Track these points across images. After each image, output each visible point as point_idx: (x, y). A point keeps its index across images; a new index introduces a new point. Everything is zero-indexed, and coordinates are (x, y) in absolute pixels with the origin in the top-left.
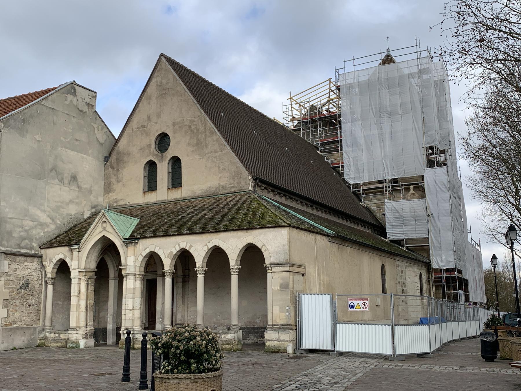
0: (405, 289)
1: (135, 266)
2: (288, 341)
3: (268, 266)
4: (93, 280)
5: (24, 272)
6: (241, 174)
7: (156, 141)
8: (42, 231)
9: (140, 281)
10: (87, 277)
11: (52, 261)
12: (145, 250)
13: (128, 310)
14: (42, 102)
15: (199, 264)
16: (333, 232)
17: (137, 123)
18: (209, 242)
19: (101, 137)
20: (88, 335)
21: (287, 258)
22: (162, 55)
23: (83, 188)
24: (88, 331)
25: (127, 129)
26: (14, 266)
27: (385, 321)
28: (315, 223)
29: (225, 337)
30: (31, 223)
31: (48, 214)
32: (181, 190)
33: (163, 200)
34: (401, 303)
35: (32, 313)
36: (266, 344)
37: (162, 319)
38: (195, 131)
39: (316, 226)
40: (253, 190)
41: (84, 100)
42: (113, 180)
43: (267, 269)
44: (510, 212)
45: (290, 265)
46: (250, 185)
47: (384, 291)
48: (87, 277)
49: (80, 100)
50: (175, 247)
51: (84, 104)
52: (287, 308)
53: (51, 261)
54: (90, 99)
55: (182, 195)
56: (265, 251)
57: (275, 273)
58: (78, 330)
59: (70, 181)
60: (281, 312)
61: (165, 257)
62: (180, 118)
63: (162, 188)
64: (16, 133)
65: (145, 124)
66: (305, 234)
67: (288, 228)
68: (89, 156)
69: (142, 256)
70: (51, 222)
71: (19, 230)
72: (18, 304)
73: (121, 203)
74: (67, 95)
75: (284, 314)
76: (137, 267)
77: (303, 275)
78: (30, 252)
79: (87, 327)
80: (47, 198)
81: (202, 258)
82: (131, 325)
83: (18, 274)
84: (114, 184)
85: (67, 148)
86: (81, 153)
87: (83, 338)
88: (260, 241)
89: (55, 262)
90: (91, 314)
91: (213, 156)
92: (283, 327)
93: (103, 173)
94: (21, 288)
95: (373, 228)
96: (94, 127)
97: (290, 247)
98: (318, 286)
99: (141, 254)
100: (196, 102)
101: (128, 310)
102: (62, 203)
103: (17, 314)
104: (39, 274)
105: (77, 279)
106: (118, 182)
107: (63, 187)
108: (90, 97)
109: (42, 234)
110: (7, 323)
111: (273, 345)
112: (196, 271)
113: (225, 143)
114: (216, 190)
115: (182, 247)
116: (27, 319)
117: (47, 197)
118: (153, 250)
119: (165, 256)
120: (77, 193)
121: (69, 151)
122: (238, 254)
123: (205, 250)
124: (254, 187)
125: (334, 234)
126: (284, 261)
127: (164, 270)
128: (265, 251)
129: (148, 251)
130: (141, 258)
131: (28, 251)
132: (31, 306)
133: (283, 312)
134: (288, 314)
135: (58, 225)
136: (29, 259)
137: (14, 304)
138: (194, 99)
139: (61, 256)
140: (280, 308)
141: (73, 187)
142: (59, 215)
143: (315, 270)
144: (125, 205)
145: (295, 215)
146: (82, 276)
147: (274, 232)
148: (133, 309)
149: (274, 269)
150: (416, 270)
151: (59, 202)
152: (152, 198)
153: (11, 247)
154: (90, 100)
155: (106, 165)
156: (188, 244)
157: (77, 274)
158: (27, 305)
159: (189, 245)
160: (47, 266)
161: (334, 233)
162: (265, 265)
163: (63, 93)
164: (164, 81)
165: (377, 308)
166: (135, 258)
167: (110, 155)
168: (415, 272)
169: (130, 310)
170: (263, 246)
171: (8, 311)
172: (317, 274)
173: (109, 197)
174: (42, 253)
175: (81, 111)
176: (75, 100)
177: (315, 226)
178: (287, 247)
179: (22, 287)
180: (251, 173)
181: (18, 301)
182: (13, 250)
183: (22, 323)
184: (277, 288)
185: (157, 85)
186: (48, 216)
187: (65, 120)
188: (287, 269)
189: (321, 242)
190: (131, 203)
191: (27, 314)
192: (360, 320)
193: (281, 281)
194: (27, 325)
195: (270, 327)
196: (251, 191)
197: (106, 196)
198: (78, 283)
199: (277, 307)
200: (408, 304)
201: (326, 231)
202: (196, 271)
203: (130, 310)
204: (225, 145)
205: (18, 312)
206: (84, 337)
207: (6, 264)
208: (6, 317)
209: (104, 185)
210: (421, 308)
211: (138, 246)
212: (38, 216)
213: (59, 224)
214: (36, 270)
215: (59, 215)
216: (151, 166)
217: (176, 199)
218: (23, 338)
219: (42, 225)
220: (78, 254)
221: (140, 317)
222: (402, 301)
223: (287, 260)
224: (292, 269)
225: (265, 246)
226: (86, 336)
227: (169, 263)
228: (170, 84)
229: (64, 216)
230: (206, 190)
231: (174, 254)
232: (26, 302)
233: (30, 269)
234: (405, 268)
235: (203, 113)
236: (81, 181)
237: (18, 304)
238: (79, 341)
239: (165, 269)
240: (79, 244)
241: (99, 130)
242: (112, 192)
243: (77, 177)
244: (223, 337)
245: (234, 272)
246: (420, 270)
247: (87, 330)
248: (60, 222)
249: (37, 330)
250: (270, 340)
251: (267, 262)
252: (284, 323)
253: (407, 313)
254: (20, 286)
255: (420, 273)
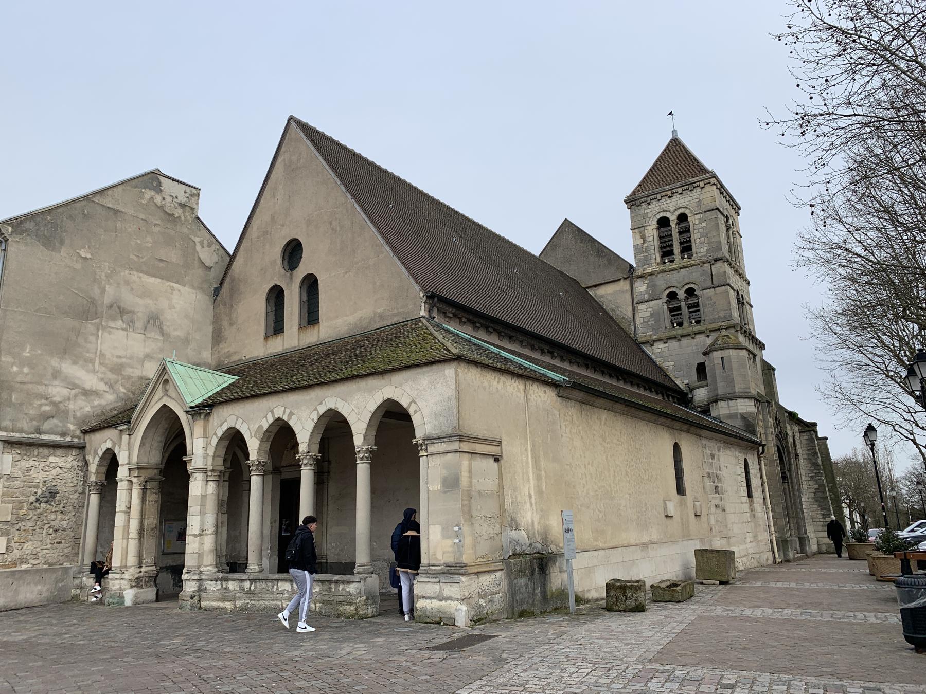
0: (720, 485)
1: (206, 456)
2: (457, 600)
3: (420, 442)
4: (155, 484)
5: (48, 473)
6: (408, 290)
7: (284, 255)
8: (89, 405)
9: (215, 482)
10: (142, 478)
11: (97, 454)
12: (221, 425)
13: (192, 535)
14: (94, 197)
15: (358, 440)
16: (565, 378)
17: (258, 229)
18: (321, 403)
19: (208, 256)
20: (142, 581)
21: (454, 425)
22: (291, 118)
23: (171, 336)
24: (141, 574)
25: (244, 241)
26: (25, 464)
27: (685, 542)
28: (531, 364)
29: (344, 589)
30: (65, 392)
31: (100, 375)
32: (319, 328)
33: (292, 348)
34: (713, 509)
35: (60, 543)
36: (417, 605)
37: (270, 549)
38: (338, 229)
39: (533, 368)
40: (427, 316)
41: (175, 200)
42: (225, 323)
43: (419, 448)
44: (884, 363)
45: (462, 438)
46: (423, 308)
47: (681, 490)
48: (142, 478)
49: (169, 199)
50: (266, 417)
51: (177, 205)
52: (456, 529)
53: (96, 453)
54: (188, 197)
55: (319, 337)
56: (415, 412)
57: (434, 457)
58: (124, 573)
59: (147, 324)
60: (445, 537)
61: (251, 437)
62: (316, 211)
63: (291, 327)
64: (38, 243)
65: (268, 229)
66: (499, 379)
67: (455, 364)
68: (184, 286)
69: (217, 437)
70: (105, 388)
71: (39, 403)
72: (31, 528)
73: (235, 358)
74: (143, 190)
75: (449, 542)
76: (209, 458)
77: (497, 460)
78: (62, 439)
79: (140, 567)
80: (101, 351)
81: (309, 434)
82: (196, 564)
83: (33, 476)
84: (225, 329)
85: (142, 272)
86: (169, 280)
87: (132, 587)
88: (405, 394)
89: (100, 453)
90: (151, 543)
91: (365, 266)
92: (449, 568)
93: (210, 314)
94: (37, 500)
95: (666, 393)
96: (194, 241)
97: (459, 399)
98: (532, 482)
99: (215, 434)
100: (339, 182)
101: (192, 535)
102: (131, 358)
103: (28, 547)
104: (79, 475)
105: (126, 482)
106: (231, 324)
107: (132, 334)
108: (187, 195)
109: (88, 409)
110: (7, 563)
111: (428, 608)
112: (299, 460)
113: (382, 241)
114: (370, 323)
115: (277, 416)
116: (52, 555)
117: (99, 349)
118: (233, 425)
119: (251, 434)
120: (160, 345)
121: (145, 276)
122: (367, 422)
123: (313, 420)
124: (429, 311)
125: (567, 382)
126: (450, 431)
127: (249, 460)
128: (415, 412)
129: (225, 427)
130: (215, 441)
131: (58, 438)
132: (60, 531)
133: (449, 537)
134: (458, 541)
135: (122, 395)
136: (59, 452)
137: (22, 528)
138: (336, 178)
139: (109, 445)
140: (443, 529)
141: (153, 334)
142: (122, 379)
143: (526, 450)
144: (240, 360)
145: (498, 353)
146: (135, 477)
147: (430, 374)
148: (200, 535)
149: (431, 449)
150: (737, 454)
151: (124, 357)
152: (278, 345)
153: (21, 431)
154: (186, 200)
155: (216, 301)
156: (287, 410)
157: (127, 473)
158: (51, 530)
159: (288, 411)
160: (91, 462)
161: (567, 379)
162: (414, 441)
163: (136, 187)
164: (294, 158)
165: (669, 521)
166: (207, 441)
167: (221, 284)
168: (736, 457)
169: (195, 536)
170: (411, 403)
171: (9, 541)
172: (532, 458)
173: (220, 349)
174: (86, 441)
175: (169, 215)
176: (158, 199)
177: (531, 369)
178: (454, 402)
179: (41, 499)
180: (423, 289)
181: (30, 524)
182: (26, 436)
183: (39, 562)
184: (436, 486)
185: (285, 165)
186: (102, 380)
187: (139, 229)
188: (455, 446)
189: (539, 396)
190: (247, 357)
191: (49, 546)
192: (634, 544)
193: (445, 472)
194: (51, 565)
195: (425, 570)
196: (424, 317)
197: (215, 349)
198: (128, 489)
199: (436, 526)
200: (728, 510)
201: (553, 377)
202: (299, 460)
203: (195, 536)
204: (382, 245)
205: (30, 543)
206: (134, 584)
207: (6, 461)
208: (4, 552)
209: (213, 332)
210: (750, 516)
211: (211, 419)
212: (79, 378)
213: (123, 392)
214: (72, 470)
215: (122, 379)
216: (276, 296)
217: (311, 343)
218: (39, 587)
219: (87, 393)
220: (129, 439)
221: (214, 548)
222: (716, 506)
223: (455, 427)
224: (465, 446)
225: (415, 403)
226: (138, 582)
227: (257, 447)
228: (302, 161)
229: (133, 380)
230: (356, 324)
231: (265, 429)
232: (49, 525)
233: (60, 468)
234: (719, 450)
235: (350, 197)
236: (168, 324)
237: (31, 528)
238: (124, 592)
239: (250, 458)
240: (129, 422)
241: (203, 247)
242: (223, 342)
243: (161, 318)
244: (340, 590)
245: (362, 459)
246: (745, 454)
247: (141, 572)
248: (125, 389)
249: (71, 572)
250: (424, 597)
251: (419, 434)
252: (451, 559)
253: (726, 526)
254: (37, 496)
255: (745, 459)
